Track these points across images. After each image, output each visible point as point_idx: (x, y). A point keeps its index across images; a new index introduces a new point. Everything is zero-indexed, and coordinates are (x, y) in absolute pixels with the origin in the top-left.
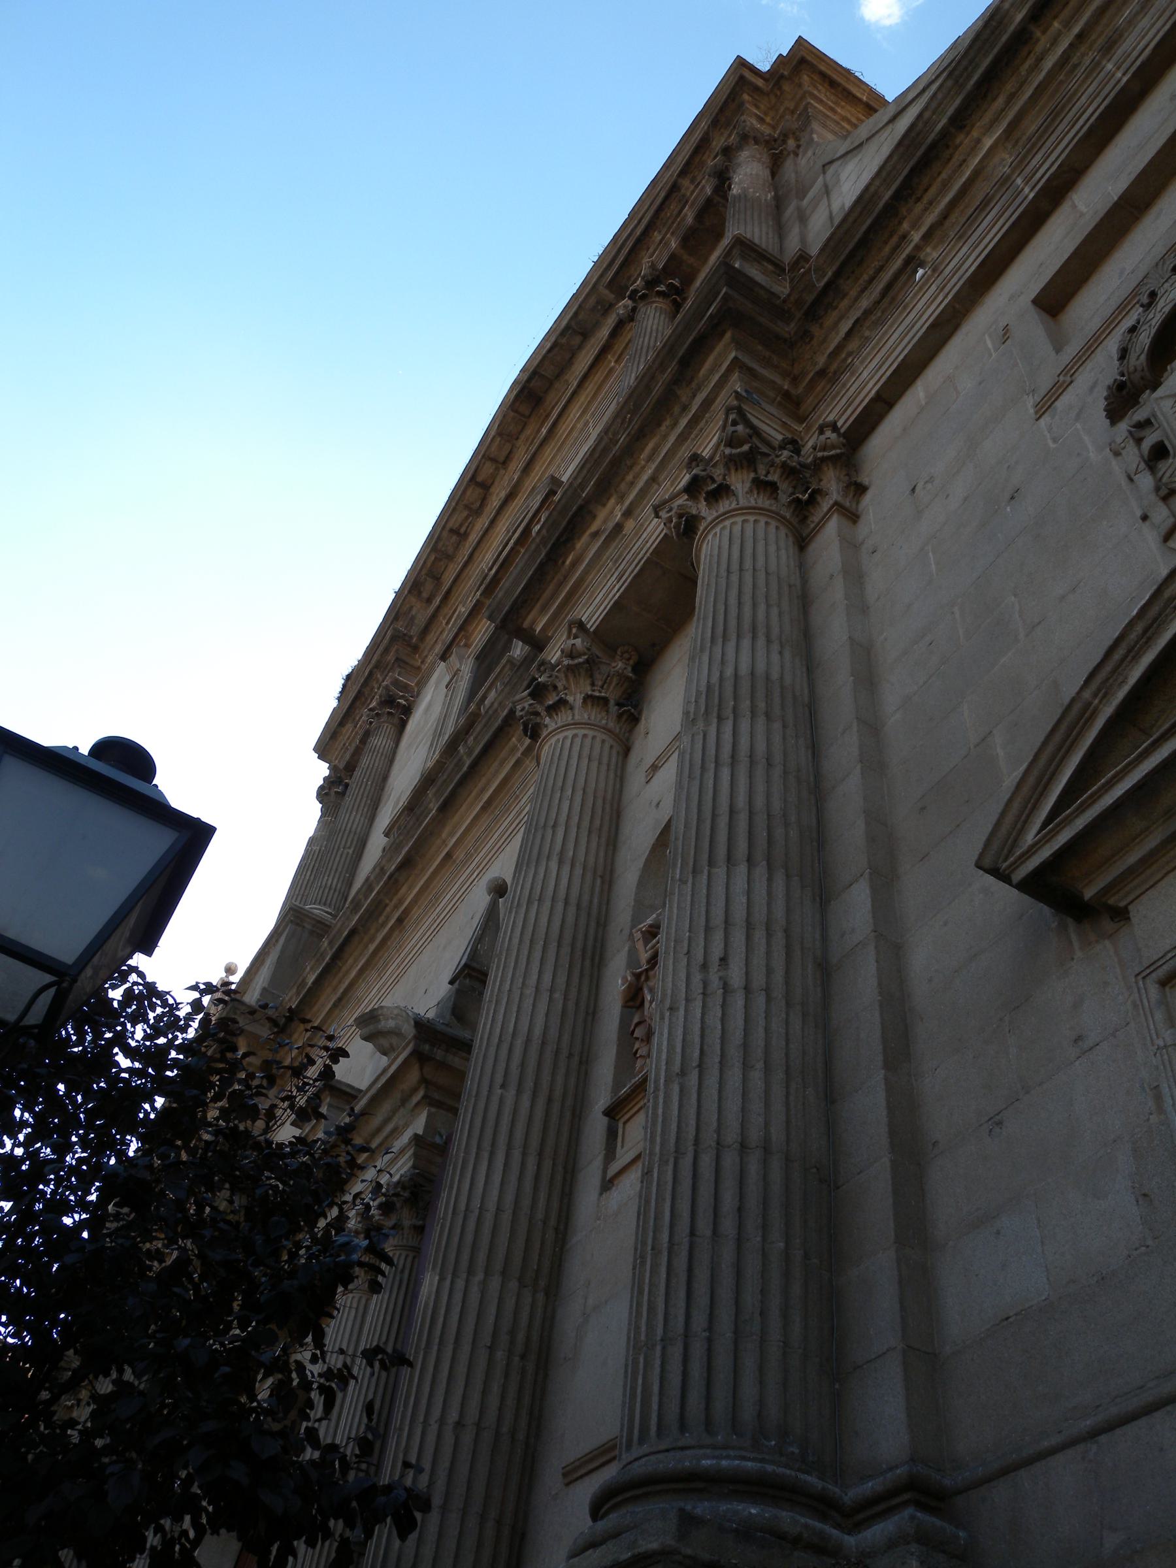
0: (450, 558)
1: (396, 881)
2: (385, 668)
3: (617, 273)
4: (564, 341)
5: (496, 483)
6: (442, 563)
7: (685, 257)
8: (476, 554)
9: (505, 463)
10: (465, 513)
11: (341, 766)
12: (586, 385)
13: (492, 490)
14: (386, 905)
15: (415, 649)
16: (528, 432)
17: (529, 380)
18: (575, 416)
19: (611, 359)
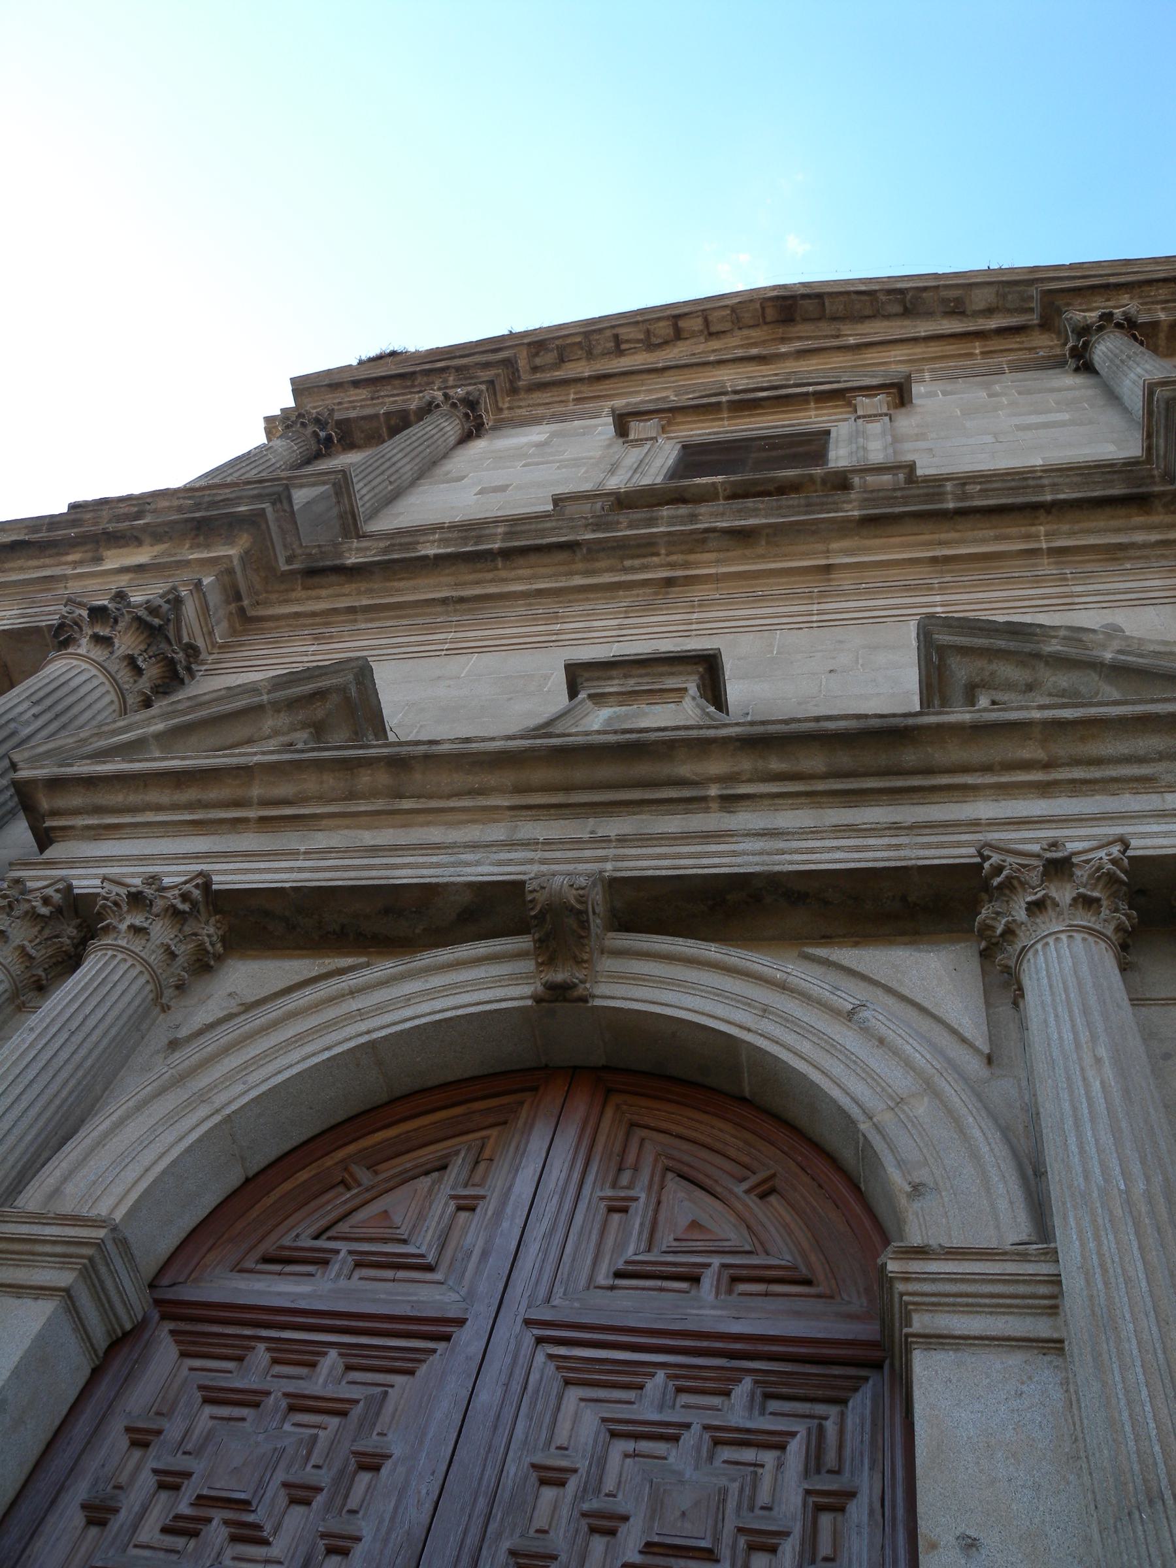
0: (590, 355)
1: (704, 541)
2: (466, 379)
3: (1062, 290)
4: (883, 298)
5: (688, 342)
6: (580, 352)
7: (1162, 335)
8: (671, 372)
9: (712, 335)
10: (642, 336)
11: (338, 416)
12: (932, 344)
13: (680, 343)
14: (657, 554)
15: (514, 391)
16: (755, 333)
17: (805, 296)
18: (895, 356)
19: (977, 348)
